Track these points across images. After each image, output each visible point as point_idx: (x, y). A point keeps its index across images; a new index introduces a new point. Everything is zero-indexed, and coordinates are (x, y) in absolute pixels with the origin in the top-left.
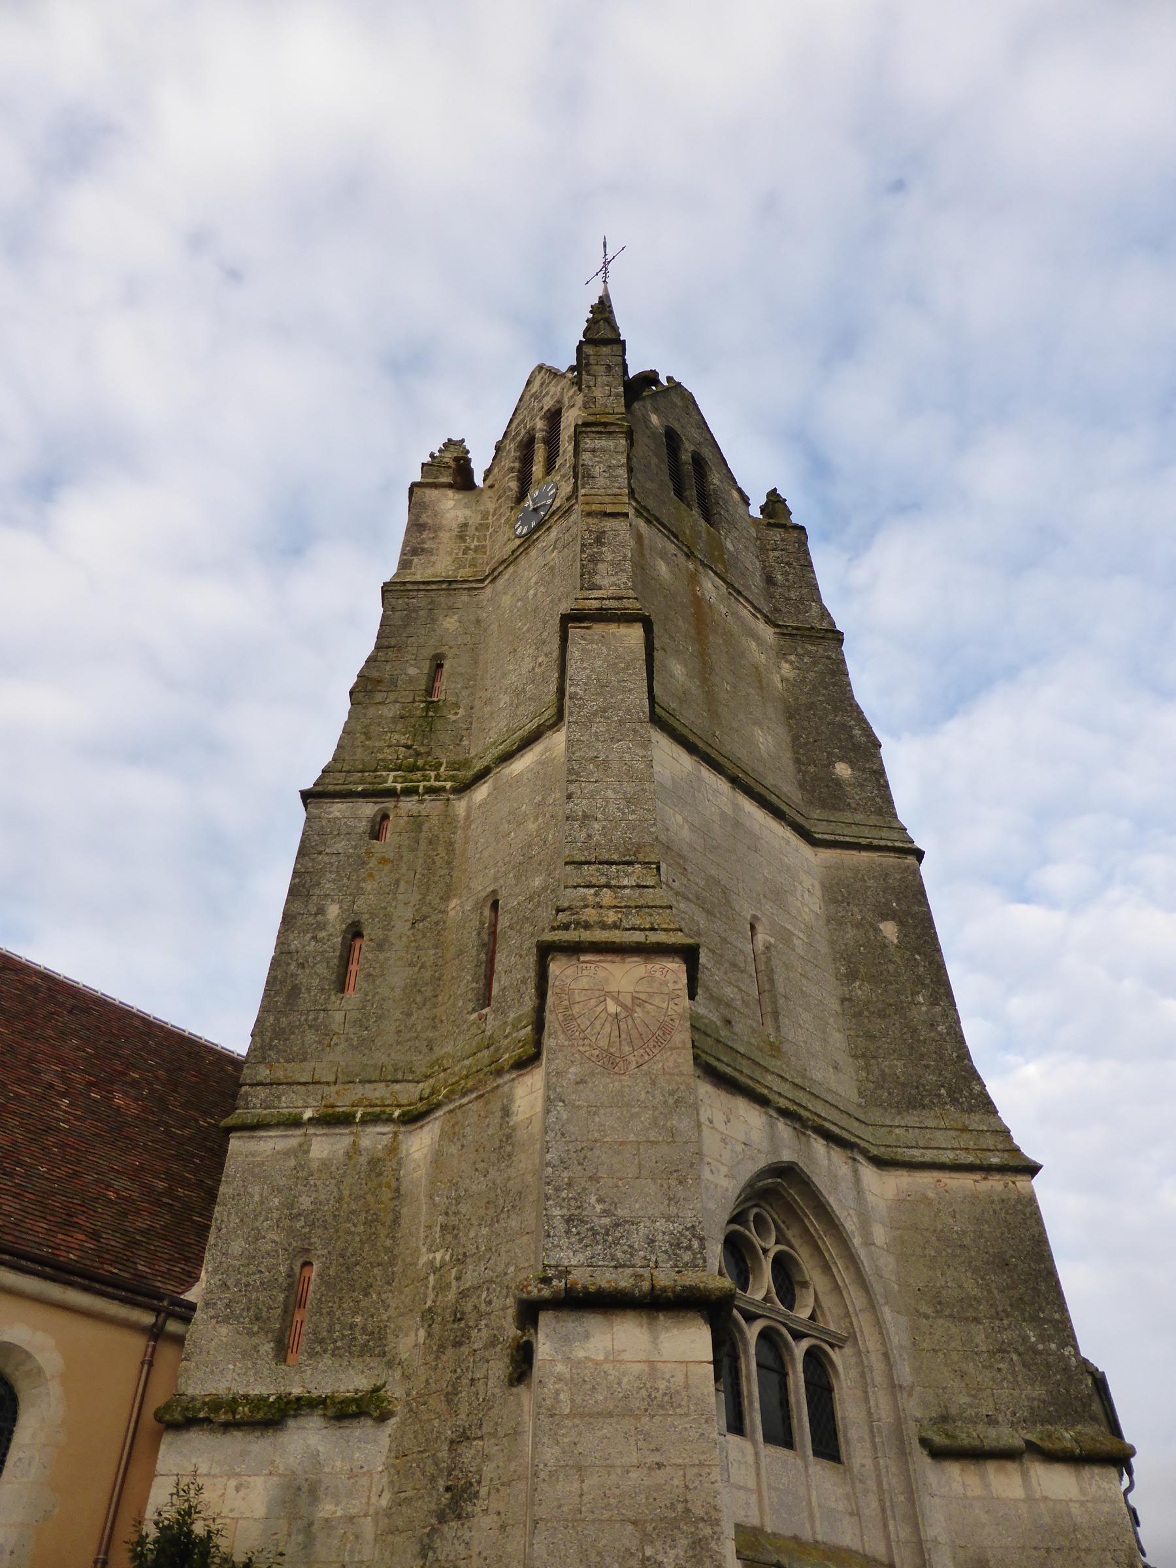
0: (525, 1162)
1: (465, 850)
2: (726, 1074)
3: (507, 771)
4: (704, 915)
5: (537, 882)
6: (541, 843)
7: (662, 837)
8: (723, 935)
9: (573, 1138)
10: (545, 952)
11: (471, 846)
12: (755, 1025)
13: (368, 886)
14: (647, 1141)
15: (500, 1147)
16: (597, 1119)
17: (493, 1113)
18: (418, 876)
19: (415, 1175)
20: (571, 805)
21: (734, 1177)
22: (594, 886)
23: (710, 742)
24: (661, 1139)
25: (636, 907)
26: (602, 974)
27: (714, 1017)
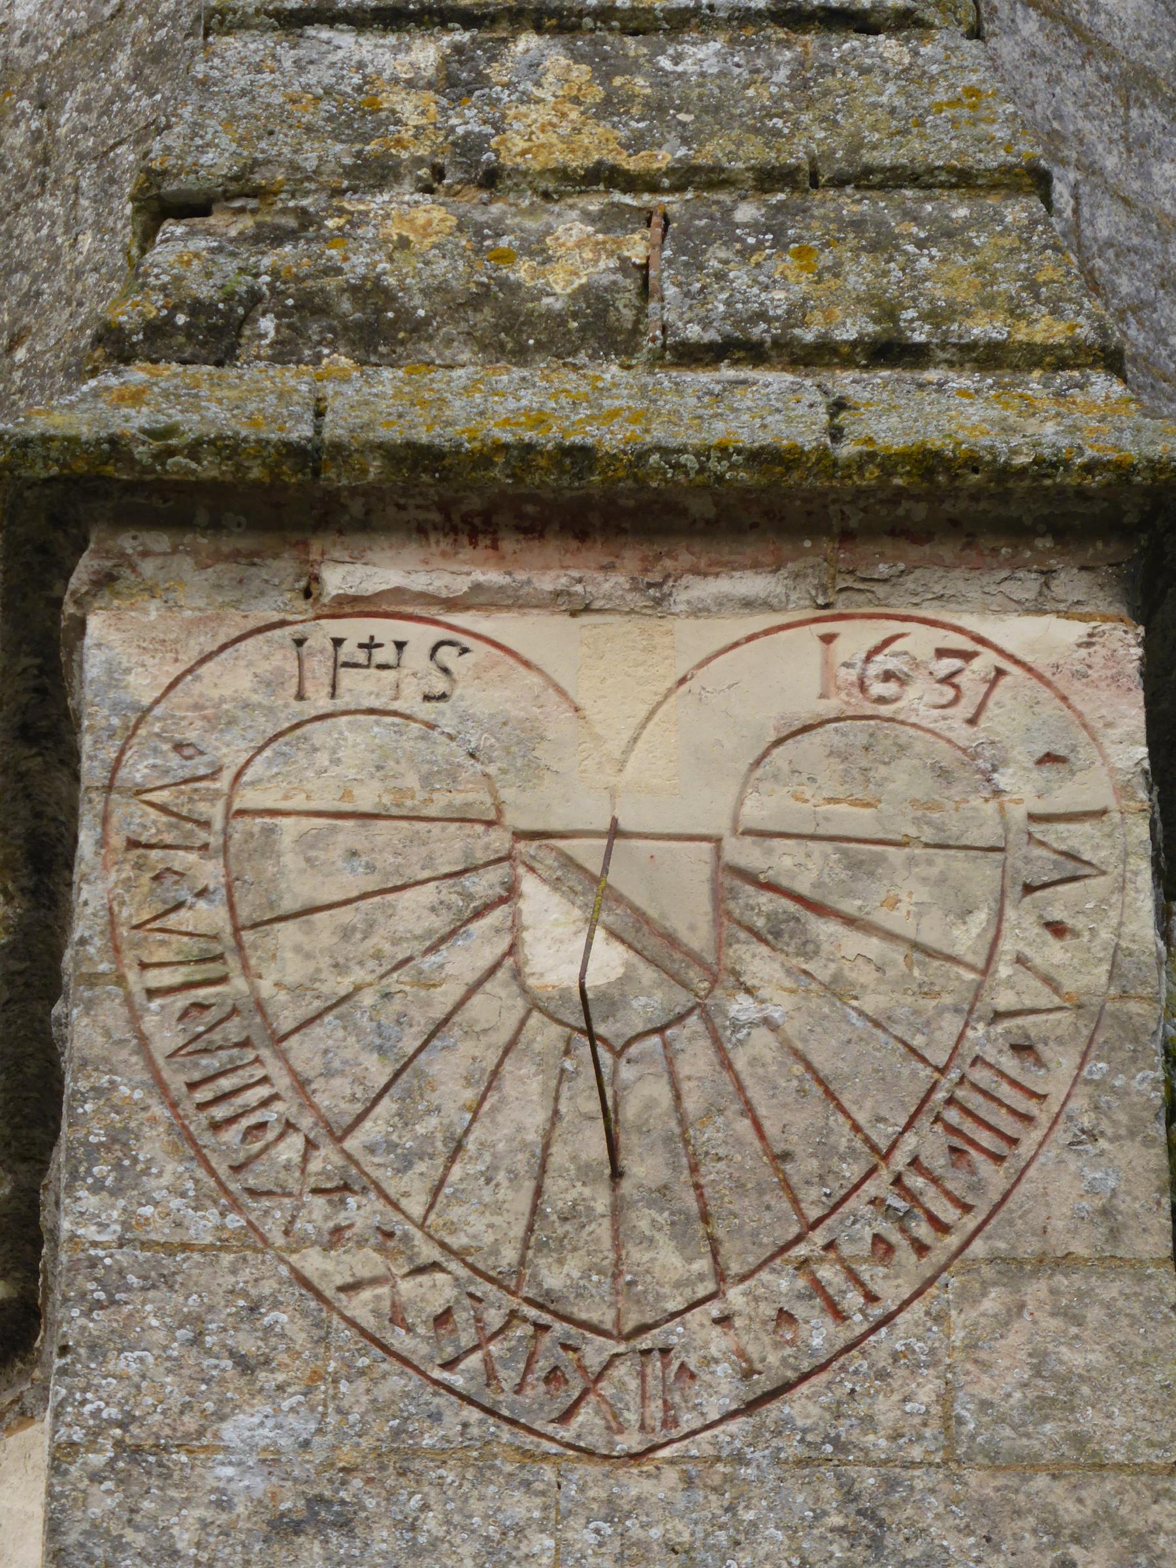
25: (768, 179)
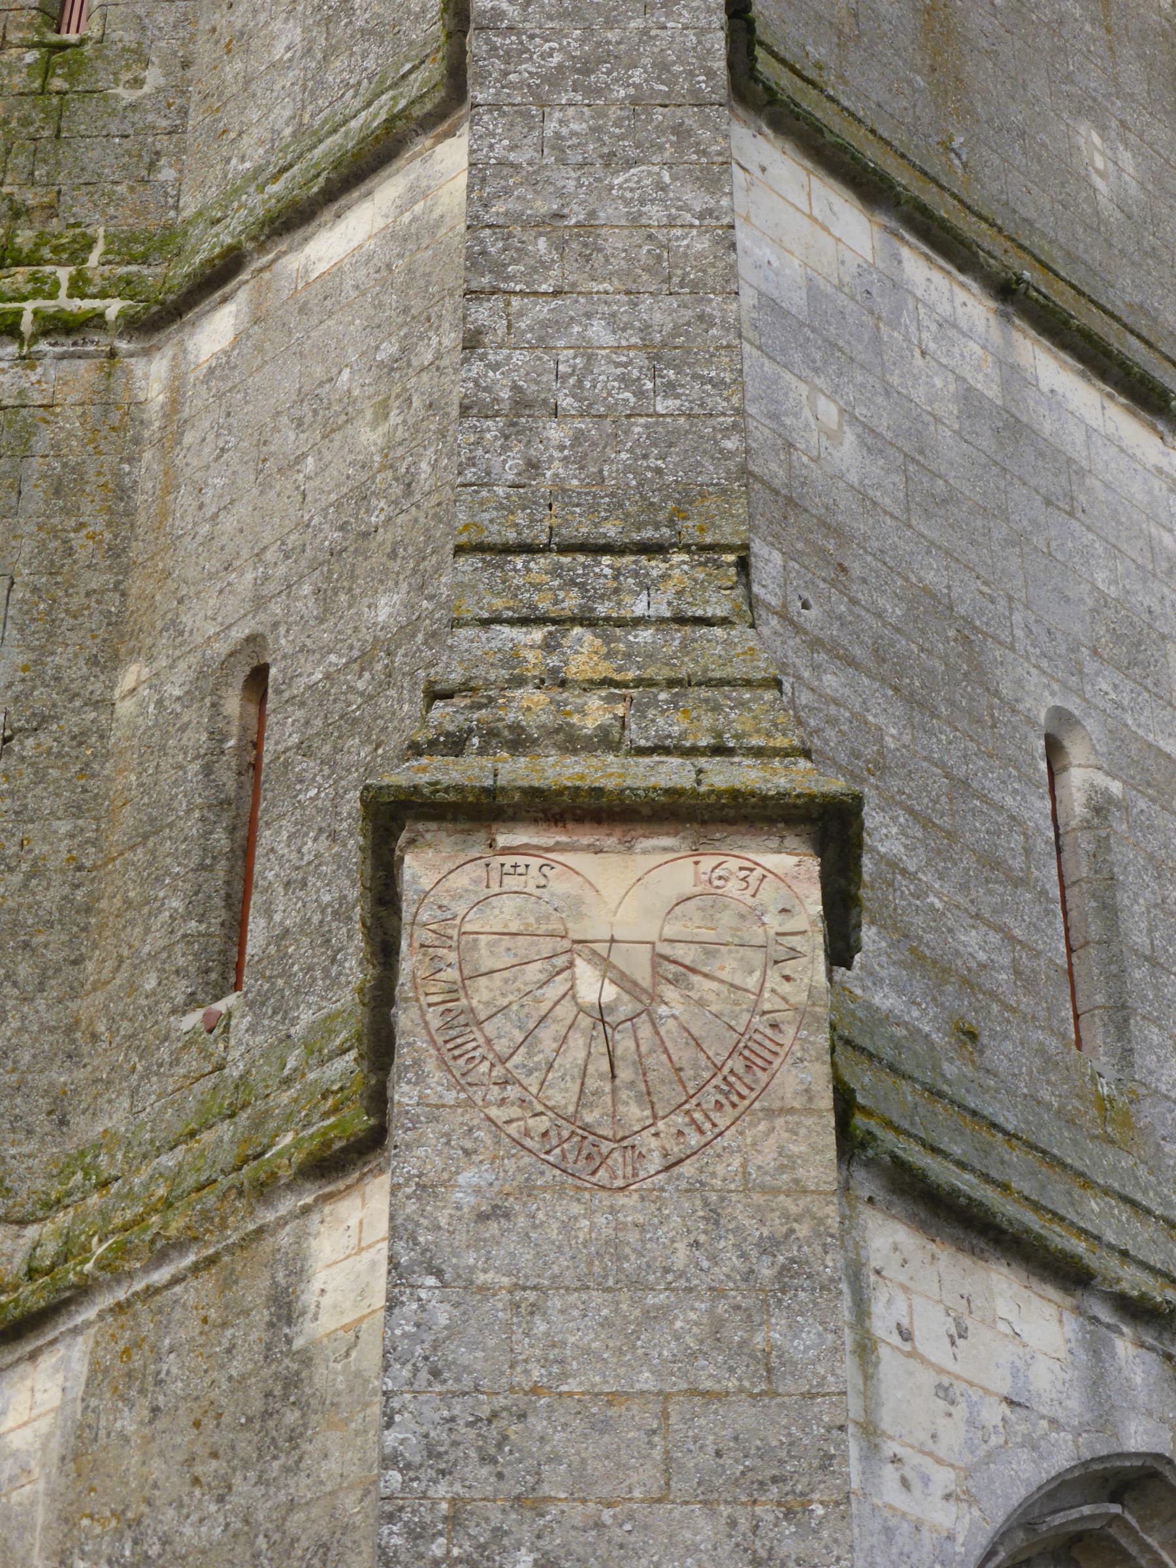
0: (338, 1458)
1: (164, 514)
2: (955, 1192)
3: (293, 263)
4: (899, 709)
5: (386, 609)
6: (397, 490)
7: (772, 468)
8: (961, 772)
9: (467, 1382)
10: (391, 819)
11: (185, 499)
12: (1052, 1044)
14: (693, 1392)
15: (267, 1414)
16: (541, 1327)
17: (246, 1313)
18: (19, 594)
19: (15, 1497)
20: (477, 367)
21: (971, 1499)
22: (542, 621)
23: (934, 169)
24: (732, 1384)
25: (671, 683)
26: (561, 885)
27: (926, 1021)
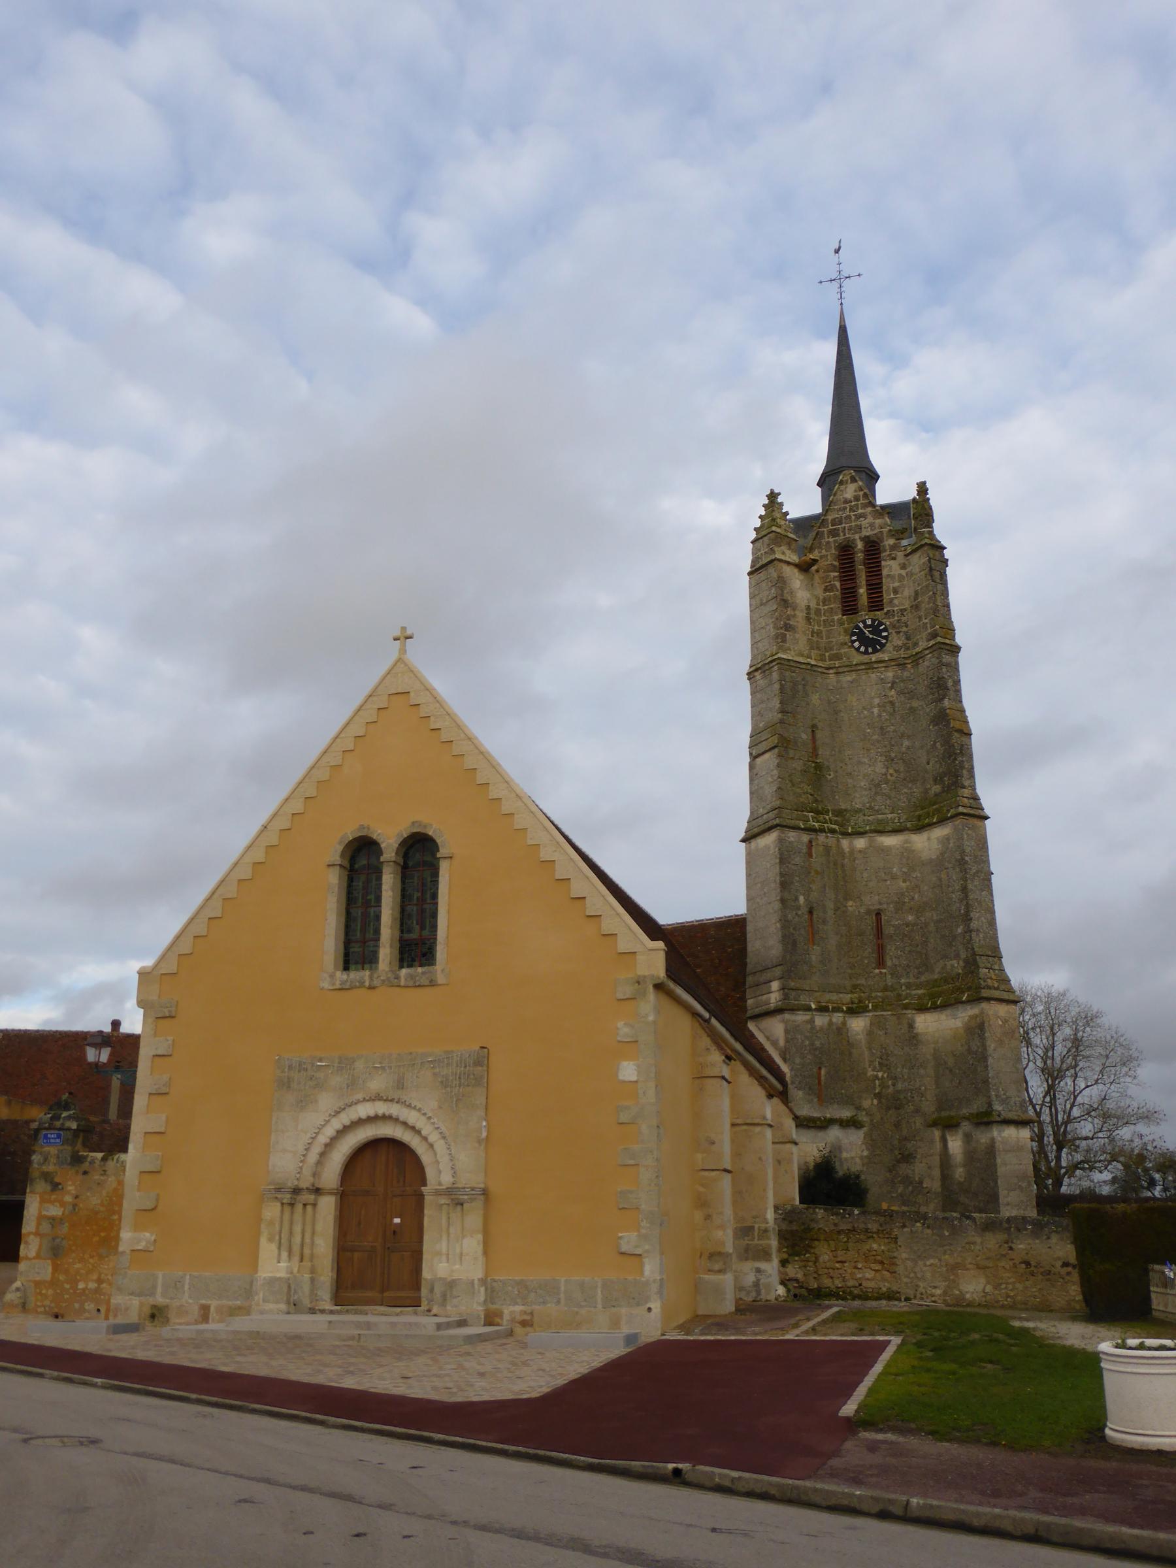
13: (814, 887)
